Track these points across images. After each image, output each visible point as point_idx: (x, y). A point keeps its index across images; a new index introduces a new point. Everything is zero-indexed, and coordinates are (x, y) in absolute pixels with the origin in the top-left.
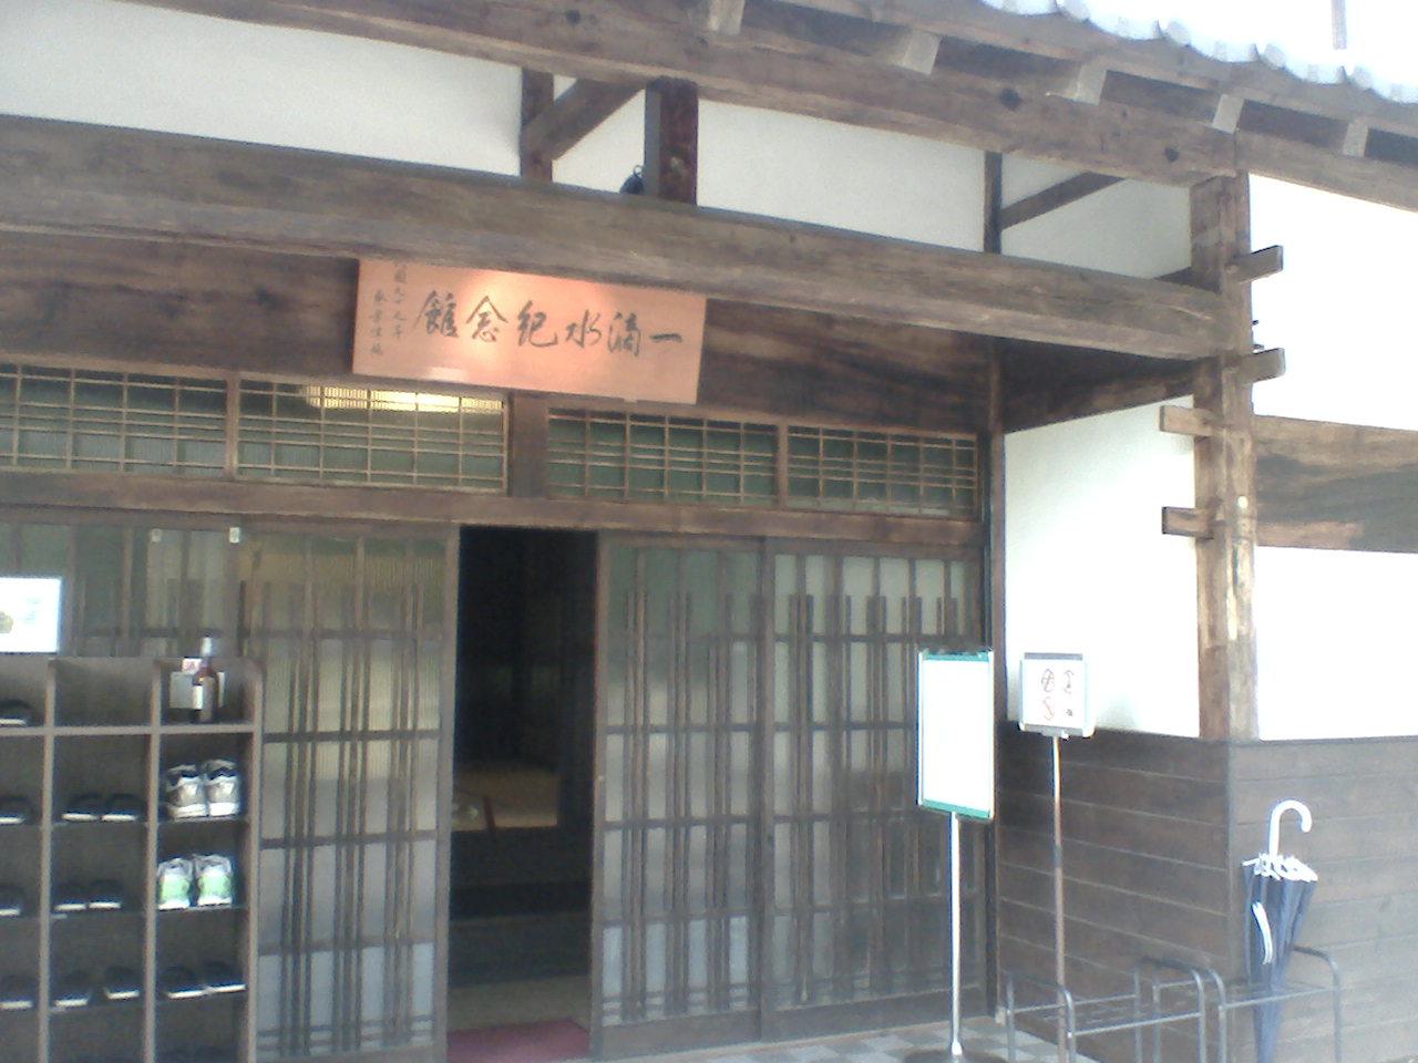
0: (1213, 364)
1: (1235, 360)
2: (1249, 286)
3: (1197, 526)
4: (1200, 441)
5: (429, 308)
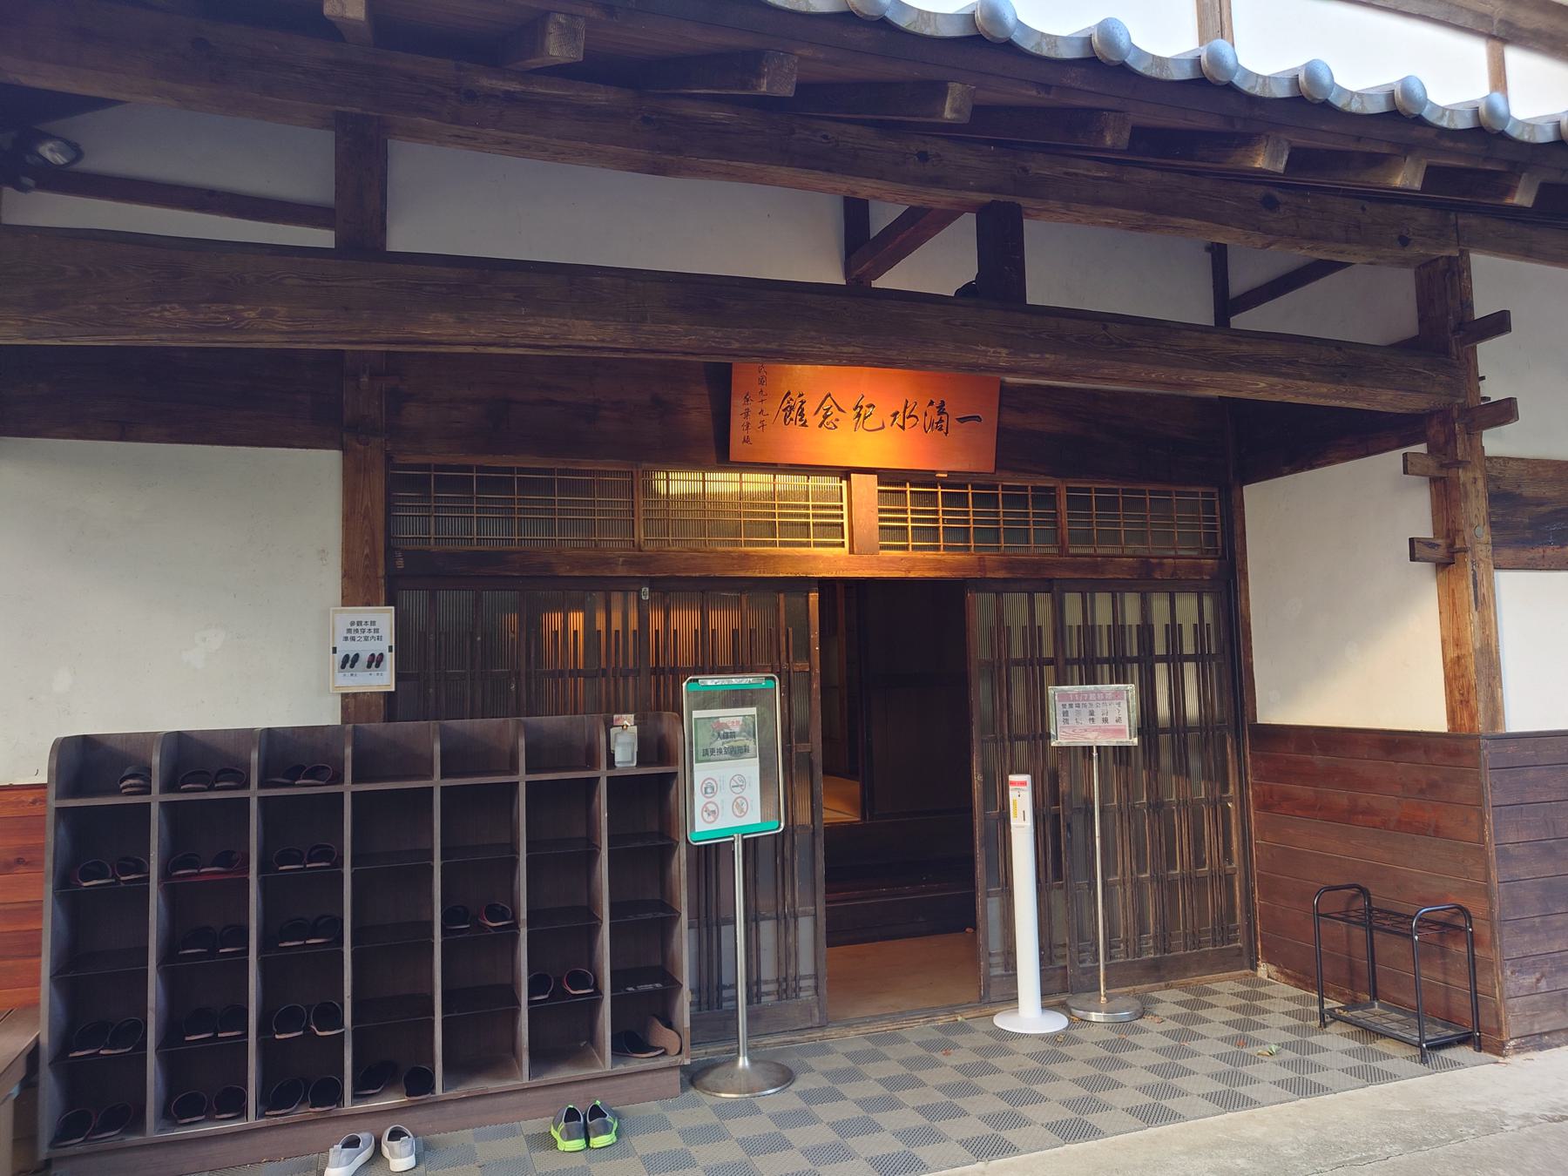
0: (1443, 415)
1: (1466, 411)
2: (1474, 349)
3: (1440, 553)
4: (1433, 481)
5: (784, 406)
